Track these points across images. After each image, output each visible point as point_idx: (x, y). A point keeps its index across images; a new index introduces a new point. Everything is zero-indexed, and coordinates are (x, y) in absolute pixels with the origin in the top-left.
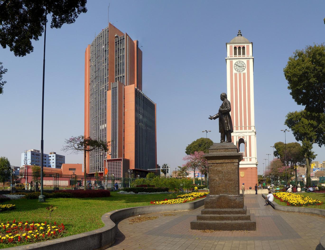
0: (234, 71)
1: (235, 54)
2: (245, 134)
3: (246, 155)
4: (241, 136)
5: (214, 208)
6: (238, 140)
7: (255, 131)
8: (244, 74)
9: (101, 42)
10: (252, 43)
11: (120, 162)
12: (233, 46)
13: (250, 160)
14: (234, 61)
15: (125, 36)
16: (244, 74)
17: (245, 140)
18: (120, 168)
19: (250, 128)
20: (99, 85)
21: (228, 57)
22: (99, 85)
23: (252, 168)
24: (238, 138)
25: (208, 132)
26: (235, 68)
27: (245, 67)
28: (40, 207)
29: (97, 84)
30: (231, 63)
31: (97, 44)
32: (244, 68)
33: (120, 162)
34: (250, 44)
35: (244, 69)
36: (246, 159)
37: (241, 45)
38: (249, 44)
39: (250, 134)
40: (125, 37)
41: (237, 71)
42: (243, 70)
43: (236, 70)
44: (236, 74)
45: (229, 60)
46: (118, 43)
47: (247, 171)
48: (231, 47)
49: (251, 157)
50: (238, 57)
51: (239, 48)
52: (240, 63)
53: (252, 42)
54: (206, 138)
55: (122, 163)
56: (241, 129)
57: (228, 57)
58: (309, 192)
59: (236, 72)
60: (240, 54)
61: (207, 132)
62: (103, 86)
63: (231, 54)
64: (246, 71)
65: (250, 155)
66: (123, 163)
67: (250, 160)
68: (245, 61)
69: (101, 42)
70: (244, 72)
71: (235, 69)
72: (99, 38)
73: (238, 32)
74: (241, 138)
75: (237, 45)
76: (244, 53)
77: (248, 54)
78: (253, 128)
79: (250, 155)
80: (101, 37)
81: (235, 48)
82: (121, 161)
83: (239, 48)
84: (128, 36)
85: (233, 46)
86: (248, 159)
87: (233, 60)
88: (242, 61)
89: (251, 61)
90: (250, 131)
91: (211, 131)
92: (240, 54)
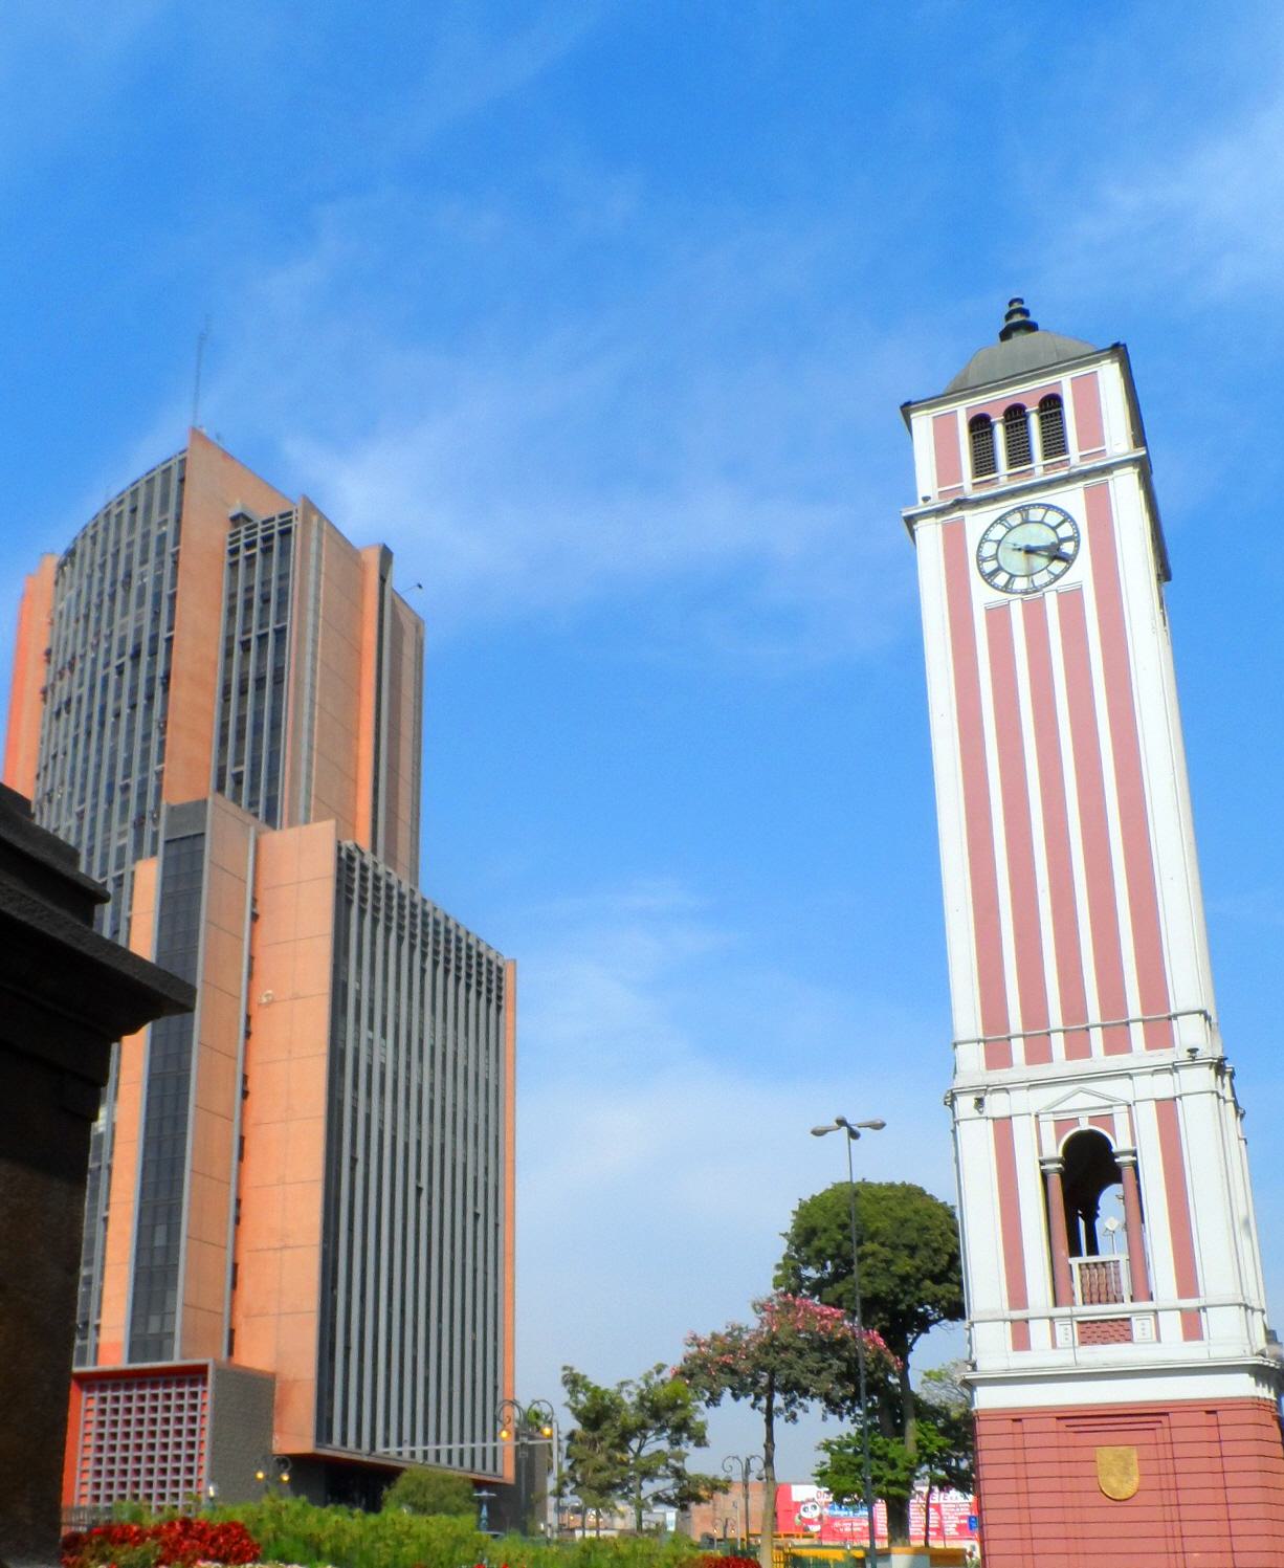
0: (982, 596)
1: (984, 463)
2: (1119, 1089)
4: (1082, 1108)
6: (1054, 1150)
7: (1211, 1049)
8: (1071, 602)
9: (130, 544)
10: (1119, 351)
11: (194, 1395)
12: (962, 411)
13: (1192, 1327)
14: (976, 522)
15: (300, 515)
16: (1071, 602)
17: (1120, 1143)
18: (191, 1458)
19: (1160, 1031)
20: (93, 820)
21: (921, 502)
22: (93, 820)
23: (1211, 1409)
24: (1048, 1129)
25: (861, 1131)
26: (1067, 525)
27: (1077, 546)
29: (81, 815)
30: (954, 540)
31: (104, 553)
33: (194, 1395)
34: (1104, 358)
36: (1150, 1324)
37: (1027, 392)
38: (1097, 361)
39: (1164, 1086)
40: (299, 523)
41: (1006, 589)
43: (995, 587)
44: (998, 618)
45: (932, 520)
46: (250, 559)
47: (1163, 1435)
48: (944, 429)
51: (1015, 414)
53: (1116, 346)
55: (208, 1399)
56: (1038, 1052)
57: (926, 499)
59: (999, 597)
61: (854, 1135)
62: (122, 834)
63: (946, 469)
64: (1081, 573)
65: (1187, 1282)
66: (216, 1402)
67: (1192, 1327)
68: (1072, 499)
69: (130, 544)
71: (988, 577)
72: (119, 516)
73: (1011, 303)
74: (1084, 1125)
75: (993, 402)
76: (1055, 444)
77: (1093, 432)
78: (1190, 1033)
79: (1187, 1282)
80: (134, 511)
81: (980, 425)
82: (204, 1383)
84: (315, 519)
86: (1172, 1324)
87: (967, 514)
88: (1039, 505)
89: (1126, 488)
90: (1165, 1057)
91: (882, 1125)
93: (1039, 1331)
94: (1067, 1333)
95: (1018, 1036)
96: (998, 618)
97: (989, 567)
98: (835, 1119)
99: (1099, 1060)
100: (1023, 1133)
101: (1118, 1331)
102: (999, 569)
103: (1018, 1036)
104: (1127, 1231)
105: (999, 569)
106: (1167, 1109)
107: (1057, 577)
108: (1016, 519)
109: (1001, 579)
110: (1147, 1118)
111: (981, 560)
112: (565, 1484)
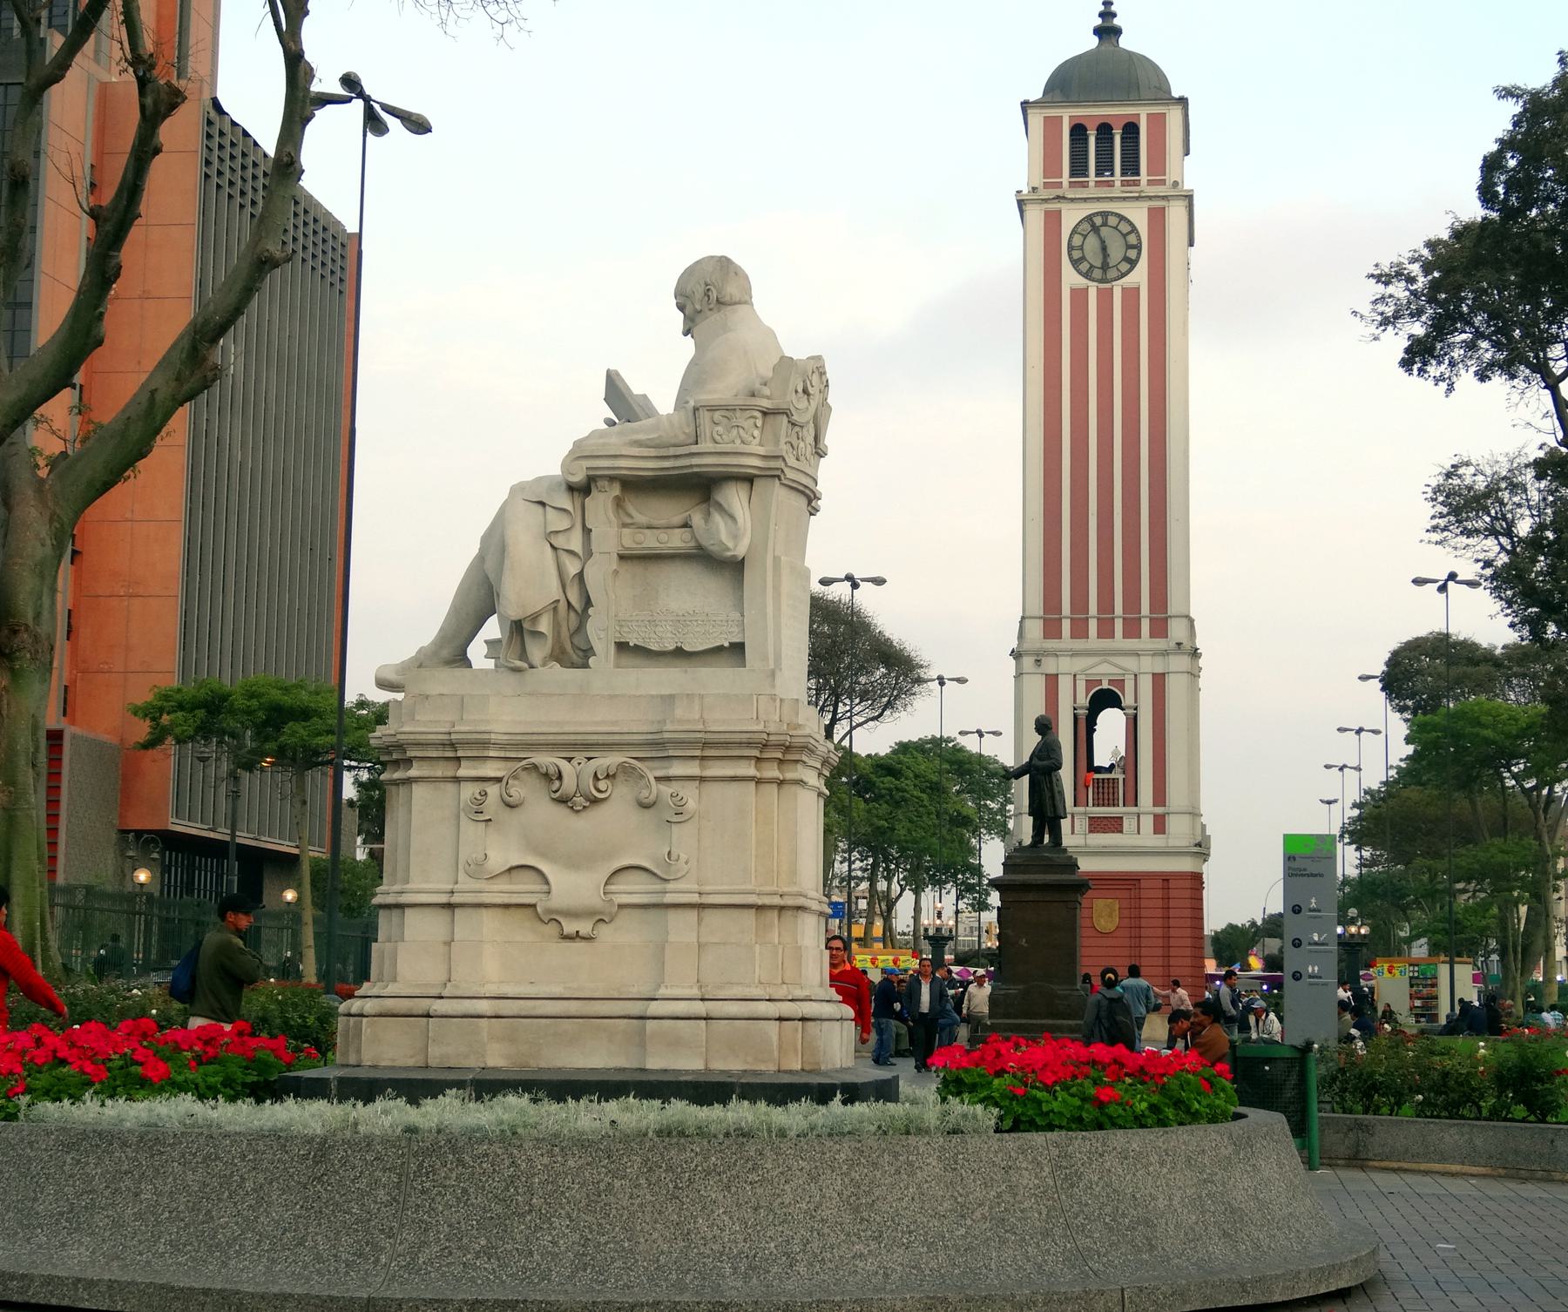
2: (1129, 663)
8: (1131, 295)
16: (1131, 295)
27: (1139, 254)
32: (1132, 254)
35: (1133, 263)
41: (1087, 275)
44: (1079, 296)
50: (1093, 192)
51: (1105, 130)
56: (1080, 631)
59: (1081, 281)
60: (1105, 166)
70: (1129, 280)
71: (1075, 263)
76: (1131, 167)
81: (1078, 131)
83: (1105, 130)
85: (1067, 116)
86: (1147, 823)
92: (1105, 166)
96: (1079, 296)
97: (1077, 255)
99: (1093, 641)
100: (1065, 685)
101: (1115, 825)
102: (1083, 258)
105: (1083, 258)
106: (1159, 680)
107: (1124, 275)
108: (1132, 239)
109: (1084, 267)
111: (1071, 248)
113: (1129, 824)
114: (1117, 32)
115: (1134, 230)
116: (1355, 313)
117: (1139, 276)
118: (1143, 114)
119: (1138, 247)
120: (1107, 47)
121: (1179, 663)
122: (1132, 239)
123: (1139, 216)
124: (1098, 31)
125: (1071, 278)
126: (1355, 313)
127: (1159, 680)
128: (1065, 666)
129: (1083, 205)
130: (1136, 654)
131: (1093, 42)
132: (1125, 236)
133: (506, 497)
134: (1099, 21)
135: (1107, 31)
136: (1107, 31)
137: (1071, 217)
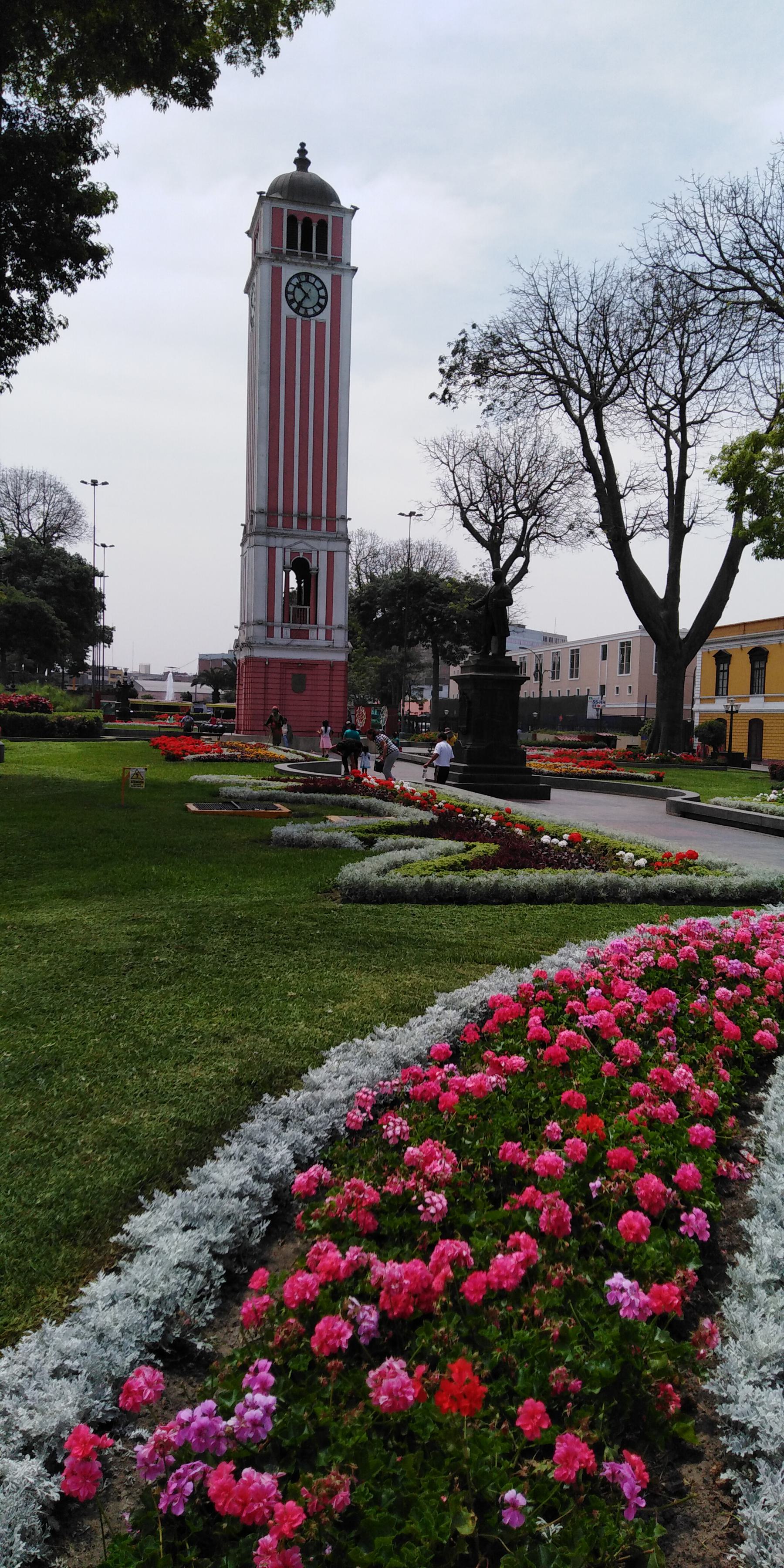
2: (314, 543)
3: (312, 620)
5: (371, 796)
8: (320, 326)
16: (320, 326)
17: (313, 565)
24: (288, 554)
28: (242, 798)
32: (322, 301)
35: (323, 307)
41: (296, 311)
42: (318, 309)
44: (291, 322)
49: (329, 627)
51: (307, 223)
52: (320, 297)
54: (537, 695)
58: (723, 767)
59: (292, 314)
71: (290, 303)
81: (292, 220)
83: (307, 223)
85: (287, 208)
86: (322, 634)
92: (307, 246)
93: (277, 631)
94: (287, 632)
95: (340, 627)
96: (291, 322)
97: (290, 297)
98: (115, 263)
100: (279, 553)
101: (304, 635)
103: (340, 627)
104: (496, 963)
106: (330, 554)
108: (322, 293)
110: (323, 556)
111: (287, 292)
112: (128, 1234)
113: (312, 634)
114: (308, 163)
115: (324, 287)
116: (83, 482)
117: (325, 316)
118: (330, 215)
119: (326, 298)
120: (301, 174)
121: (341, 545)
122: (322, 293)
123: (326, 278)
124: (296, 161)
125: (286, 311)
126: (83, 482)
127: (330, 554)
128: (277, 542)
129: (294, 267)
130: (319, 538)
131: (293, 168)
132: (318, 290)
133: (353, 221)
134: (297, 155)
135: (302, 162)
136: (302, 162)
137: (288, 272)
